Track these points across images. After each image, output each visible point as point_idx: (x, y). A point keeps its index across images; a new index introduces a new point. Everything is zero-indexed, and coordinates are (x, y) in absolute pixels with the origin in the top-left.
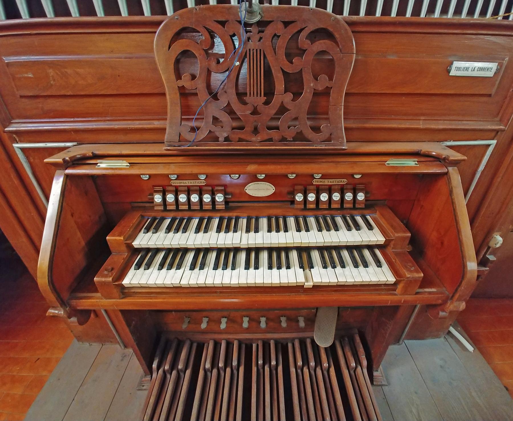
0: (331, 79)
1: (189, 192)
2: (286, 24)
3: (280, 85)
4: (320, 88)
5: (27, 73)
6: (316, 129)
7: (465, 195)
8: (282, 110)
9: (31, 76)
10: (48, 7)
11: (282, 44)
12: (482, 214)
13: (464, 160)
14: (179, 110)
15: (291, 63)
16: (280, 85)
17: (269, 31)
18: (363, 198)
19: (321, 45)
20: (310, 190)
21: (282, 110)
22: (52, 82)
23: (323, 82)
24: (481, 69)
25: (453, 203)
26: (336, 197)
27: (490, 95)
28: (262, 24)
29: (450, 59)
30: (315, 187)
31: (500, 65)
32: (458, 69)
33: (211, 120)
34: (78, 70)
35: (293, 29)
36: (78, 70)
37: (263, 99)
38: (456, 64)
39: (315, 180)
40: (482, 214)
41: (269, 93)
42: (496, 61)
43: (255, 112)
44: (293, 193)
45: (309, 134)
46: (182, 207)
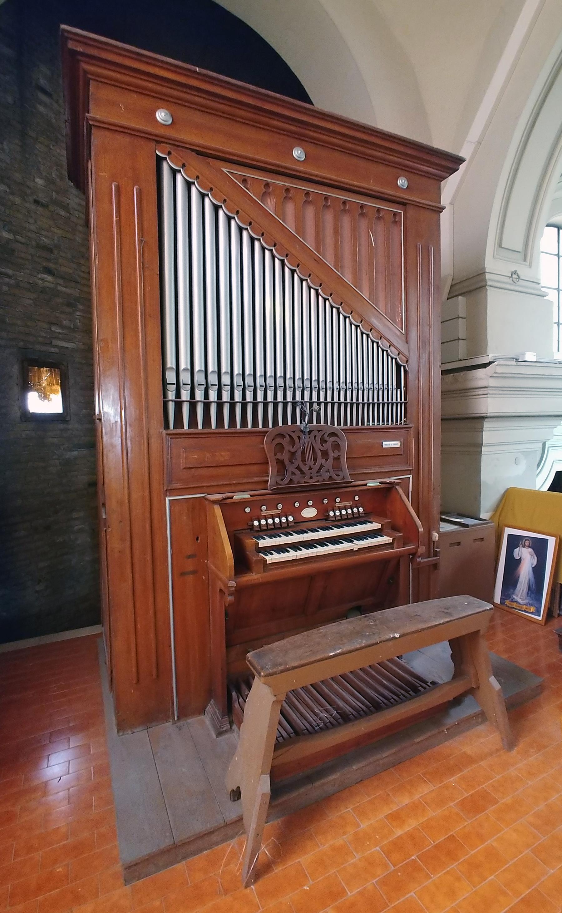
0: (339, 451)
1: (273, 517)
2: (319, 431)
3: (319, 455)
4: (336, 456)
5: (194, 456)
6: (338, 475)
7: (409, 500)
8: (322, 466)
9: (196, 457)
10: (172, 413)
11: (318, 439)
12: (86, 147)
13: (401, 482)
14: (276, 471)
15: (323, 446)
16: (319, 455)
17: (312, 435)
18: (362, 510)
19: (334, 438)
20: (335, 509)
21: (322, 466)
22: (206, 460)
23: (336, 454)
24: (394, 444)
25: (403, 501)
26: (349, 511)
27: (401, 455)
28: (310, 432)
29: (382, 441)
30: (337, 508)
31: (401, 442)
32: (386, 445)
33: (291, 473)
34: (222, 453)
35: (321, 433)
36: (222, 453)
37: (313, 462)
38: (384, 443)
39: (337, 503)
40: (86, 147)
41: (315, 460)
42: (359, 708)
43: (310, 469)
44: (328, 512)
45: (334, 476)
46: (270, 527)
